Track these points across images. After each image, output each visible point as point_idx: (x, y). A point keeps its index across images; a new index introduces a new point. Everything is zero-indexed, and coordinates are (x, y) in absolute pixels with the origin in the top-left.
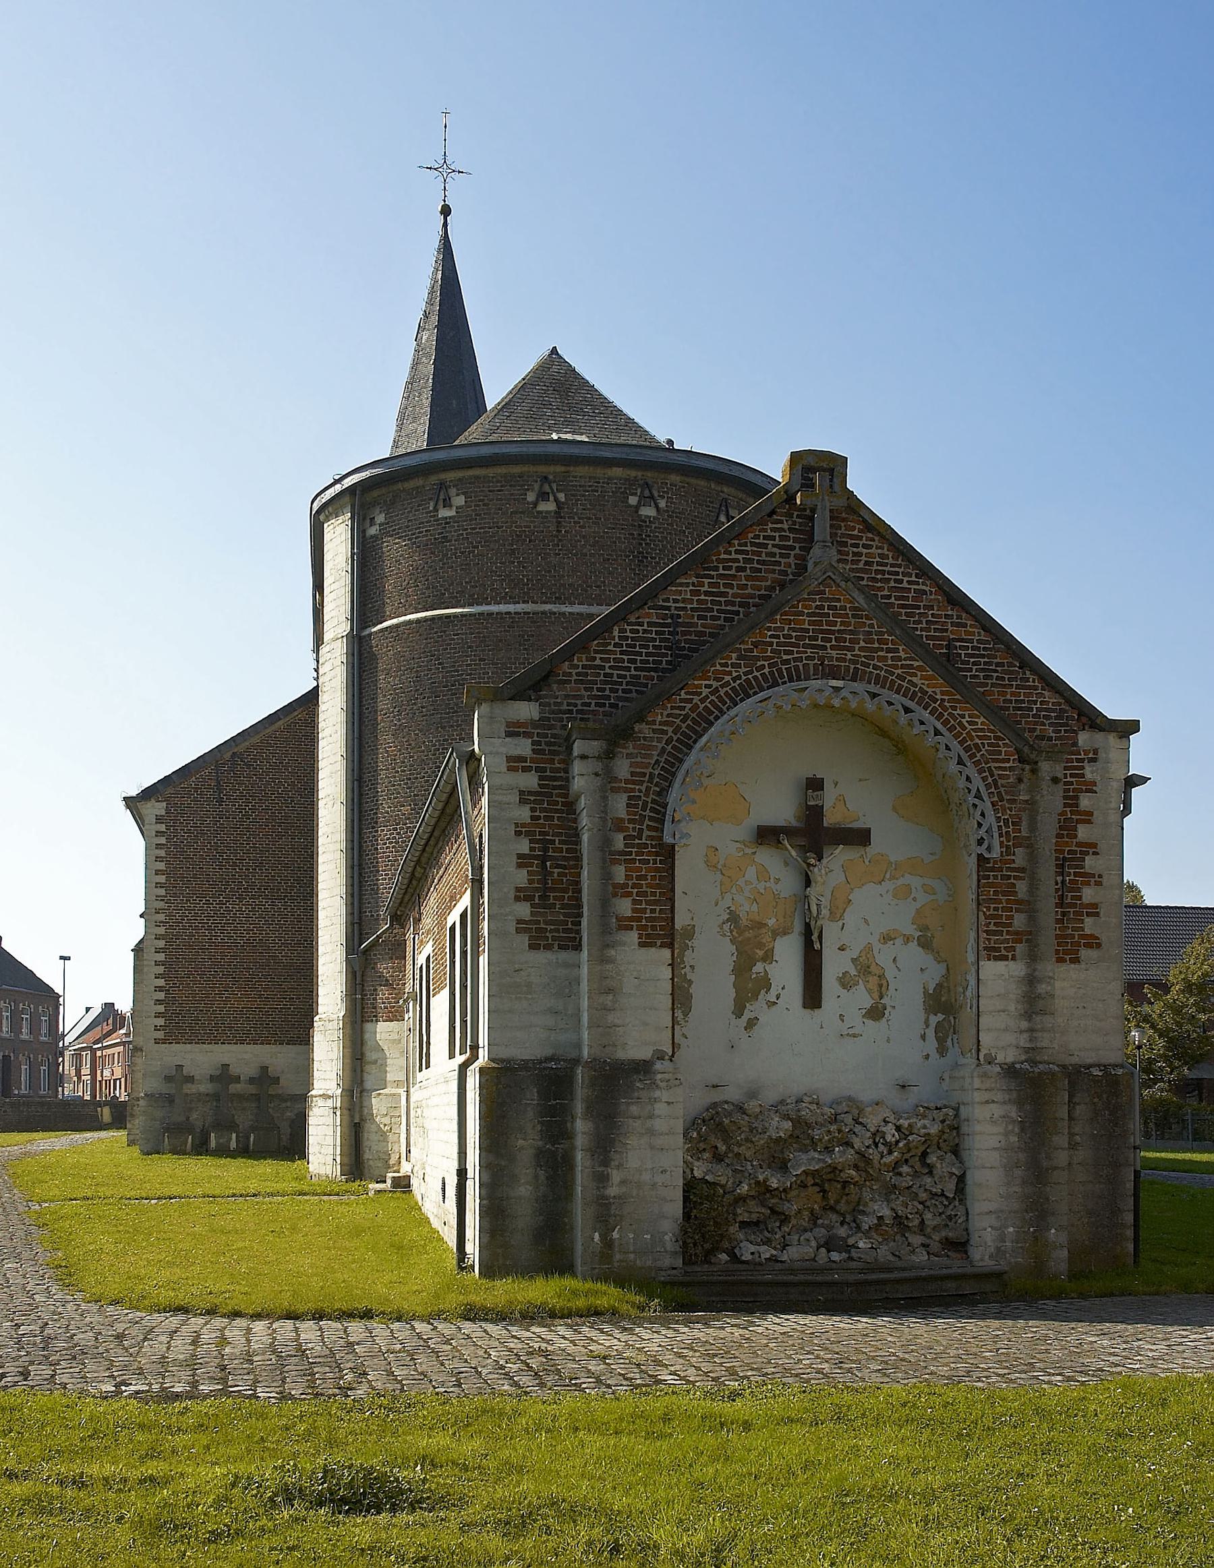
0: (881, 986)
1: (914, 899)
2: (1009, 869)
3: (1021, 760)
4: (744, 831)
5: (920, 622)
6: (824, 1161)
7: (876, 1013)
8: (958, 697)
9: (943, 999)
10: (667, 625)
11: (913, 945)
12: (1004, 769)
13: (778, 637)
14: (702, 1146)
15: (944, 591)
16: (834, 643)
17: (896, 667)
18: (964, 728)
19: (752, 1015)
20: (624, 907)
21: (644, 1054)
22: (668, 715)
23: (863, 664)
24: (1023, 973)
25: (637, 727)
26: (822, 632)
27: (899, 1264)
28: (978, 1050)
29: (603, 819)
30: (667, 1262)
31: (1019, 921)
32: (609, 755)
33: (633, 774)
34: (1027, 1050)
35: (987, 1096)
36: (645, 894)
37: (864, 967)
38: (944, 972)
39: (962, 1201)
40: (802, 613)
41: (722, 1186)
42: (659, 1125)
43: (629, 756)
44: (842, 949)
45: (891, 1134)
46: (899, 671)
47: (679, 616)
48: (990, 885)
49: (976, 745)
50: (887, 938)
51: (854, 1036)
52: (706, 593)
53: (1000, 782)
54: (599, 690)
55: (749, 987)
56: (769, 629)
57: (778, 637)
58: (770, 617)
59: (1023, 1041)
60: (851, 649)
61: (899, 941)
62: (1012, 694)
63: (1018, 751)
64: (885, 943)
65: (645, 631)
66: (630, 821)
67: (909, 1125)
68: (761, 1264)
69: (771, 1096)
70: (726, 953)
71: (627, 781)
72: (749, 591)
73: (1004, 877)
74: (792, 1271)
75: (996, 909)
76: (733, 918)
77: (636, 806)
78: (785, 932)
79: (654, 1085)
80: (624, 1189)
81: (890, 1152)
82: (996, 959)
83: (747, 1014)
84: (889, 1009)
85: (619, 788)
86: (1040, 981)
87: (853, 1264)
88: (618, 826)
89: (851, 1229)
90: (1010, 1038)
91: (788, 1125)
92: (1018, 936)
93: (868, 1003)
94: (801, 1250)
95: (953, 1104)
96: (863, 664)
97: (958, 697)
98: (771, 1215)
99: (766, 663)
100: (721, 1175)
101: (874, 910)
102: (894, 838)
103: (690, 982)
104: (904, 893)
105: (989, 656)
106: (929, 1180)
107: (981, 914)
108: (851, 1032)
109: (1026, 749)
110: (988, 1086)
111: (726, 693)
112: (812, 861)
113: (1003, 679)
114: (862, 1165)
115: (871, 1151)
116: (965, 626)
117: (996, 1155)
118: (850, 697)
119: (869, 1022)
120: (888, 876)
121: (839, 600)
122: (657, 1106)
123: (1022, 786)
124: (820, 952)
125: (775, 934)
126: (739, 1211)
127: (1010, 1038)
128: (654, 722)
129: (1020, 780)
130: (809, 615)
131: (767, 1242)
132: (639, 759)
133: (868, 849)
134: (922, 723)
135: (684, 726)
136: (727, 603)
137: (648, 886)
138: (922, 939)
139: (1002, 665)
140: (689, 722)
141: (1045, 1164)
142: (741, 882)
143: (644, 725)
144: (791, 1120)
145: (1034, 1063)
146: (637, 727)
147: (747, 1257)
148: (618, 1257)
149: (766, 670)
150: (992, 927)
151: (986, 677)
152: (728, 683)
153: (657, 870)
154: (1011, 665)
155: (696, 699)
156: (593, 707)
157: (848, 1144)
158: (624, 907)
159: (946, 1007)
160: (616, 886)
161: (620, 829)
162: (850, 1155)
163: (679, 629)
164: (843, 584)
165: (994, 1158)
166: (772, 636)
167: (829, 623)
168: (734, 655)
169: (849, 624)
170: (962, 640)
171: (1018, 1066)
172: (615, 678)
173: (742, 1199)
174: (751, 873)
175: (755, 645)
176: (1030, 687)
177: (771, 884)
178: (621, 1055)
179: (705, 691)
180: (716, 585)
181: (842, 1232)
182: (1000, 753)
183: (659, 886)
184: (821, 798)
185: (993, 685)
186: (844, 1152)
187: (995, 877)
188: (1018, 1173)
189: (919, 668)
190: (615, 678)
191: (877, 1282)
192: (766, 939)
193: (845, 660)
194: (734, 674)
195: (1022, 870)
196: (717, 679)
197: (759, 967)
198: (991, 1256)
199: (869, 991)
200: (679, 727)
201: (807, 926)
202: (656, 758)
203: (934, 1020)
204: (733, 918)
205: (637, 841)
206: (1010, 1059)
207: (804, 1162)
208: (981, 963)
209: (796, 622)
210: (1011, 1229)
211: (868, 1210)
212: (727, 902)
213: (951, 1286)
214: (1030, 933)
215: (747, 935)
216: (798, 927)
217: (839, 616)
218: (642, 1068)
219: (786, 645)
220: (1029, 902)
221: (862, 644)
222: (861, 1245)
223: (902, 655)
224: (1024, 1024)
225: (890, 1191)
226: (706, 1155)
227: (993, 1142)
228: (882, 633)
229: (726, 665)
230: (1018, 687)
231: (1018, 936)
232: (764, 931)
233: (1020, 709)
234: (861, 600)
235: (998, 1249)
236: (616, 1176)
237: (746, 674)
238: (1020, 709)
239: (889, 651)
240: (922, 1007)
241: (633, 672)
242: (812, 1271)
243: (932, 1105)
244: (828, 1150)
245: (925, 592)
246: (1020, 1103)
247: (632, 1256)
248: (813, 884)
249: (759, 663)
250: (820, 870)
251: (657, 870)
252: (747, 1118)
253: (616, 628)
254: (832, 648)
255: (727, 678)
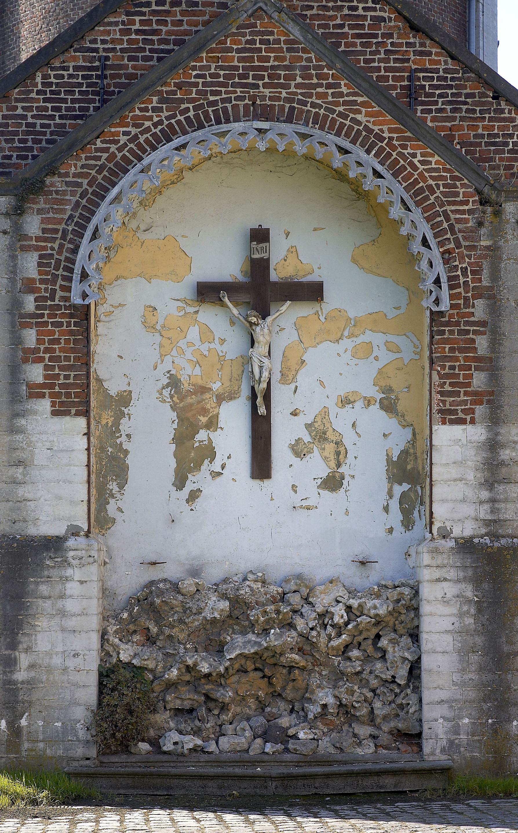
0: (338, 453)
1: (376, 358)
2: (467, 323)
3: (484, 202)
4: (185, 289)
5: (378, 52)
6: (259, 644)
7: (333, 483)
8: (408, 134)
9: (409, 467)
10: (96, 69)
11: (375, 408)
12: (463, 212)
13: (203, 76)
14: (132, 627)
15: (405, 18)
16: (266, 80)
17: (337, 104)
18: (415, 168)
19: (195, 487)
20: (36, 373)
21: (57, 529)
22: (83, 167)
23: (300, 102)
24: (483, 438)
25: (48, 180)
26: (253, 68)
27: (340, 757)
28: (431, 523)
29: (12, 281)
30: (80, 751)
31: (479, 380)
32: (18, 211)
33: (44, 231)
34: (487, 523)
35: (438, 574)
36: (58, 359)
37: (320, 433)
38: (410, 437)
39: (417, 690)
40: (230, 50)
41: (151, 671)
42: (71, 605)
43: (40, 211)
44: (294, 414)
45: (339, 614)
46: (341, 109)
47: (107, 58)
48: (447, 341)
49: (430, 187)
50: (346, 401)
51: (308, 508)
52: (137, 32)
53: (457, 226)
54: (20, 141)
55: (191, 456)
56: (194, 68)
57: (203, 76)
58: (195, 54)
59: (484, 512)
60: (286, 87)
61: (359, 404)
62: (484, 128)
63: (479, 192)
64: (343, 406)
65: (70, 76)
66: (42, 281)
67: (360, 605)
68: (182, 755)
69: (214, 574)
70: (166, 420)
71: (38, 239)
72: (185, 27)
73: (460, 332)
74: (219, 763)
75: (452, 368)
76: (174, 382)
77: (48, 265)
78: (232, 396)
79: (66, 563)
80: (32, 674)
81: (339, 635)
82: (453, 422)
83: (189, 487)
84: (347, 478)
85: (29, 246)
86: (503, 446)
87: (288, 757)
88: (29, 286)
89: (298, 718)
90: (469, 510)
91: (225, 605)
92: (478, 397)
93: (324, 472)
94: (236, 740)
95: (411, 582)
96: (300, 102)
97: (408, 134)
98: (204, 701)
99: (191, 106)
100: (149, 659)
101: (336, 369)
102: (354, 289)
103: (126, 452)
104: (365, 351)
105: (457, 87)
106: (379, 665)
107: (434, 373)
108: (305, 503)
109: (486, 190)
110: (439, 562)
111: (147, 141)
112: (254, 320)
113: (474, 111)
114: (307, 648)
115: (314, 633)
116: (430, 54)
117: (449, 638)
118: (277, 139)
119: (325, 493)
120: (346, 333)
121: (272, 33)
122: (69, 585)
123: (483, 231)
124: (267, 418)
125: (220, 399)
126: (169, 698)
127: (469, 510)
128: (67, 175)
129: (480, 224)
130: (238, 51)
131: (197, 732)
132: (51, 215)
133: (323, 305)
134: (359, 164)
135: (100, 177)
136: (161, 41)
137: (61, 350)
138: (386, 402)
139: (473, 96)
140: (105, 173)
141: (506, 649)
142: (182, 344)
143: (56, 179)
144: (228, 598)
145: (495, 536)
146: (48, 180)
147: (168, 747)
148: (26, 745)
149: (191, 114)
150: (447, 388)
151: (454, 110)
152: (148, 130)
153: (71, 333)
154: (483, 95)
155: (113, 148)
156: (14, 160)
157: (291, 626)
158: (36, 373)
159: (411, 473)
160: (27, 351)
161: (32, 290)
162: (291, 637)
163: (108, 72)
164: (276, 15)
165: (447, 642)
166: (197, 76)
167: (261, 59)
168: (155, 99)
169: (284, 59)
170: (426, 70)
171: (476, 540)
172: (38, 128)
173: (171, 685)
174: (193, 334)
175: (179, 86)
176: (505, 120)
177: (216, 345)
178: (32, 531)
179: (123, 139)
180: (149, 22)
181: (285, 721)
182: (457, 194)
183: (73, 350)
184: (266, 250)
185: (462, 119)
186: (281, 635)
187: (451, 332)
188: (475, 658)
189: (363, 104)
190: (38, 128)
191: (305, 777)
192: (211, 403)
193: (279, 99)
194: (156, 119)
195: (483, 324)
196: (135, 126)
197: (202, 435)
198: (443, 750)
199: (326, 459)
200: (94, 179)
201: (253, 388)
202: (69, 213)
203: (398, 490)
204: (174, 382)
205: (49, 303)
206: (468, 533)
207: (241, 645)
208: (435, 428)
209: (225, 59)
210: (466, 721)
211: (314, 697)
212: (167, 365)
213: (389, 783)
214: (492, 393)
215: (189, 400)
216: (245, 392)
217: (273, 50)
218: (54, 545)
219: (212, 84)
220: (491, 359)
221: (299, 80)
222: (301, 735)
223: (344, 90)
224: (485, 494)
225: (338, 676)
226: (136, 638)
227: (446, 624)
228: (321, 68)
229: (146, 110)
230: (491, 119)
231: (478, 397)
232: (207, 396)
233: (494, 144)
234: (296, 33)
235: (451, 742)
236: (24, 660)
237: (168, 118)
238: (494, 144)
239: (329, 86)
240: (385, 476)
241: (58, 121)
242: (241, 763)
243: (390, 583)
244: (266, 631)
245: (383, 19)
246: (476, 581)
247: (41, 745)
248: (256, 344)
249: (183, 106)
250: (262, 329)
251: (71, 333)
252: (180, 598)
253: (39, 74)
254: (265, 86)
255: (148, 124)
